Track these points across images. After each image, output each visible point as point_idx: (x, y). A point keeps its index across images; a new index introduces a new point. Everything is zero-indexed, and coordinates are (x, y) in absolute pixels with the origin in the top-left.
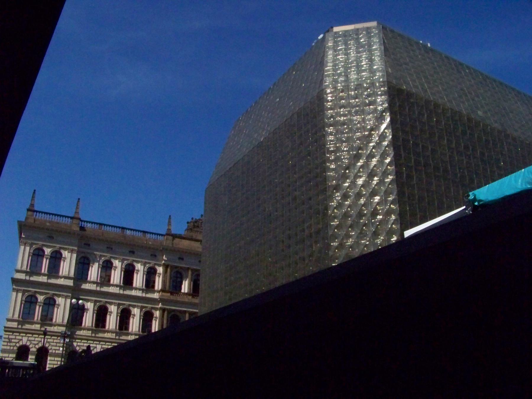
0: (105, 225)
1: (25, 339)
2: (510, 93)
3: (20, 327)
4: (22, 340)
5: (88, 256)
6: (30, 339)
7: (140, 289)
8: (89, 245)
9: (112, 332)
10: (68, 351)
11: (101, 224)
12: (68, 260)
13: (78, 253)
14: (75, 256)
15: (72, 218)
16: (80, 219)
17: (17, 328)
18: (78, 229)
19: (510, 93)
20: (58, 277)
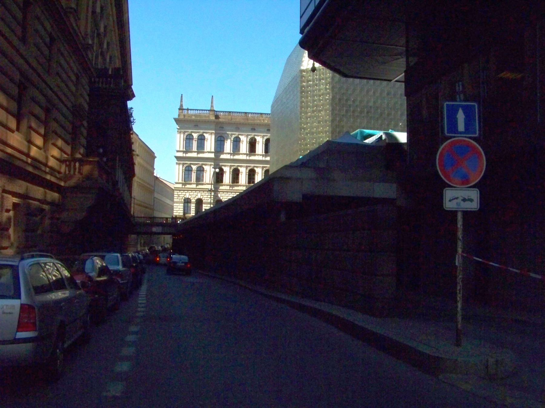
8: (197, 126)
9: (227, 185)
14: (213, 136)
16: (214, 111)
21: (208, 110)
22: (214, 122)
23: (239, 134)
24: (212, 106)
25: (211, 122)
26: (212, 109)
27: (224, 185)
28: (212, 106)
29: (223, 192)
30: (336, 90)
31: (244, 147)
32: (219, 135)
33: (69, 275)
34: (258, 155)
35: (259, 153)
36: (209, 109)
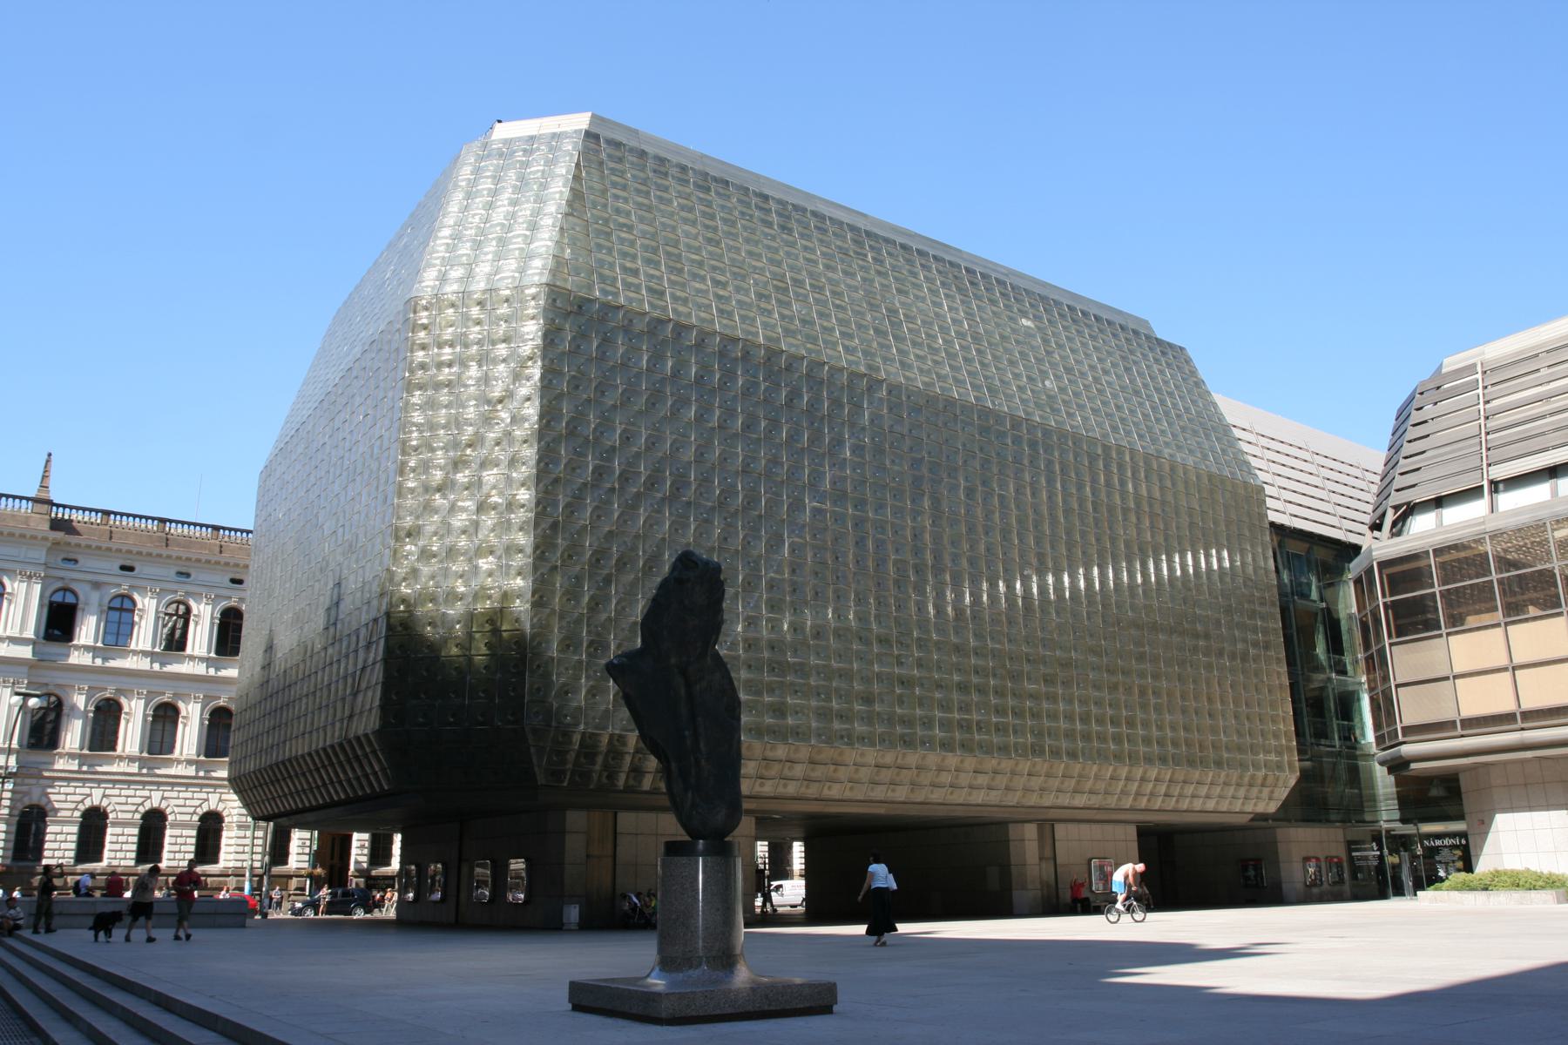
0: (171, 521)
1: (214, 798)
2: (1101, 331)
3: (85, 768)
4: (90, 795)
5: (74, 586)
6: (108, 792)
7: (201, 659)
8: (188, 575)
9: (131, 759)
10: (20, 806)
11: (107, 513)
12: (21, 600)
13: (45, 581)
14: (37, 588)
15: (36, 500)
16: (51, 503)
17: (196, 777)
18: (46, 526)
19: (1101, 331)
20: (125, 653)
21: (28, 499)
22: (45, 539)
23: (188, 594)
24: (44, 486)
25: (34, 537)
26: (43, 495)
27: (121, 758)
28: (44, 486)
29: (115, 782)
30: (556, 558)
31: (145, 634)
32: (59, 584)
33: (895, 887)
34: (192, 658)
35: (197, 653)
36: (32, 494)
